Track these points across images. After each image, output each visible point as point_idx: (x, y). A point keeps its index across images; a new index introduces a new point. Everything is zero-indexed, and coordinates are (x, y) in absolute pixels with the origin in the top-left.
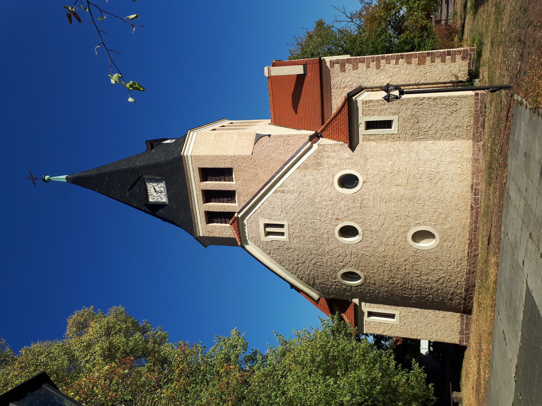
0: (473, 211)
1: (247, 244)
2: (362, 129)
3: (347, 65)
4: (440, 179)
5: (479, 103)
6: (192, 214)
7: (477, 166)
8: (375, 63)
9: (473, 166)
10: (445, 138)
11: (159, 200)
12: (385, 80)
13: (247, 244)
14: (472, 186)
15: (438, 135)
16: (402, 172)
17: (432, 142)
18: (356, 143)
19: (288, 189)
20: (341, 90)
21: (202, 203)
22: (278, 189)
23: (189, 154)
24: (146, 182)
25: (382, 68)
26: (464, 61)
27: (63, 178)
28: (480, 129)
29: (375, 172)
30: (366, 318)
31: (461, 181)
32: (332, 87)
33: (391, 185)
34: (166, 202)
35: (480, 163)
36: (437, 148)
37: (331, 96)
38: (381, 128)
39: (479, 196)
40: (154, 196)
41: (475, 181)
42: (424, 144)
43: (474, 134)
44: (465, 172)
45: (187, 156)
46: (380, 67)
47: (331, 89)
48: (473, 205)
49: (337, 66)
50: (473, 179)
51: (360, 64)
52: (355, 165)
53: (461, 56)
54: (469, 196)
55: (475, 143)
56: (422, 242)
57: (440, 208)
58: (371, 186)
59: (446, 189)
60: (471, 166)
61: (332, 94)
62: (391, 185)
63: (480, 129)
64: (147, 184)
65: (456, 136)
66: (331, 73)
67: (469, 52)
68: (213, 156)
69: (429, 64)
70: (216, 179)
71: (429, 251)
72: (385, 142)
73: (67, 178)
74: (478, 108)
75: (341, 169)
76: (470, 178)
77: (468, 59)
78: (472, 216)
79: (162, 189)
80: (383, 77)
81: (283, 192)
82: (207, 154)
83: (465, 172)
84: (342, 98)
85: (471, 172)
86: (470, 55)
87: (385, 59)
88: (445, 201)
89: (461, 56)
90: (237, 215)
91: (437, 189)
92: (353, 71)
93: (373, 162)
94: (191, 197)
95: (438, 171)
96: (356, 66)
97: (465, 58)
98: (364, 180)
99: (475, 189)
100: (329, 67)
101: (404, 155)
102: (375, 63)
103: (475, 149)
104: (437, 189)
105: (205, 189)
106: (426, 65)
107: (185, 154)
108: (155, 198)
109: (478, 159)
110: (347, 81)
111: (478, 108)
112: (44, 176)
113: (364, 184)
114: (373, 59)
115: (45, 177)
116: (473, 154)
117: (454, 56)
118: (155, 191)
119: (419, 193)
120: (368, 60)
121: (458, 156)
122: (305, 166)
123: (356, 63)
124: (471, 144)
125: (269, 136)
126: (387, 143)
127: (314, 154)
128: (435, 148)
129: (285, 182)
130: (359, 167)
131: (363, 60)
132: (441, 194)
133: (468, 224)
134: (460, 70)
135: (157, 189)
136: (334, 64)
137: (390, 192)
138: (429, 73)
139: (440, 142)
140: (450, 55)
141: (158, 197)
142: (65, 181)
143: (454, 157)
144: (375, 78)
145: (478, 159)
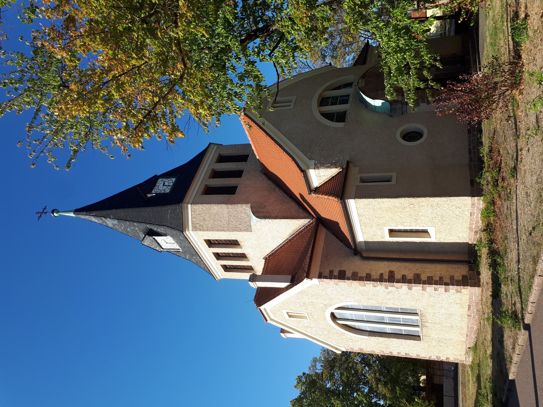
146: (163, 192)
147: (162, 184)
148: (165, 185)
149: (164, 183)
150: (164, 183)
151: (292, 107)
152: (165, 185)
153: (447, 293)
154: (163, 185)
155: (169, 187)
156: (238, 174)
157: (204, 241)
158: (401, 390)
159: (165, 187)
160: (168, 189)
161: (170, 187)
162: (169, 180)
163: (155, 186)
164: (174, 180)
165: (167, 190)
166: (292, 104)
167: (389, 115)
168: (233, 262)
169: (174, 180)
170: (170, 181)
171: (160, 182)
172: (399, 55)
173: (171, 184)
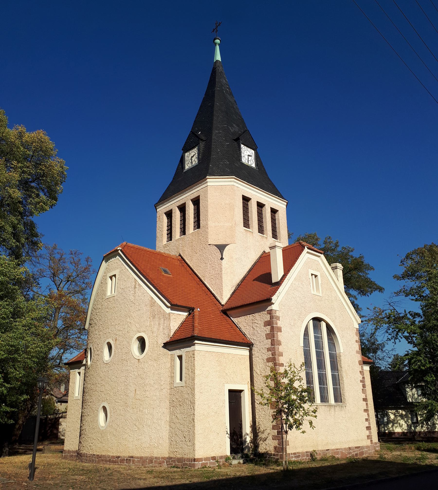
0: (116, 459)
1: (106, 262)
2: (178, 352)
3: (269, 327)
4: (138, 428)
5: (189, 463)
6: (169, 198)
7: (147, 462)
8: (271, 356)
9: (147, 458)
10: (170, 432)
11: (187, 162)
12: (259, 368)
13: (106, 262)
14: (132, 457)
15: (172, 425)
16: (145, 394)
17: (168, 420)
18: (169, 348)
19: (137, 291)
20: (251, 324)
21: (177, 205)
22: (137, 282)
23: (209, 184)
24: (197, 146)
25: (267, 364)
26: (273, 449)
27: (218, 57)
28: (174, 464)
29: (146, 369)
30: (77, 371)
31: (137, 447)
32: (253, 315)
33: (136, 385)
34: (185, 169)
35: (149, 464)
36: (163, 425)
37: (247, 315)
38: (317, 360)
39: (125, 464)
40: (189, 157)
41: (136, 459)
42: (167, 411)
43: (171, 458)
44: (143, 451)
45: (207, 182)
46: (268, 362)
47: (252, 314)
48: (120, 458)
49: (268, 318)
50: (137, 458)
51: (270, 340)
52: (151, 350)
53: (277, 445)
54: (125, 454)
55: (165, 459)
56: (105, 415)
57: (120, 430)
58: (136, 367)
59: (132, 434)
60: (147, 455)
61: (248, 316)
62: (136, 385)
63: (174, 464)
64: (197, 148)
65: (171, 442)
66: (263, 312)
67: (279, 454)
68: (207, 207)
69: (271, 413)
70: (195, 214)
71: (97, 421)
72: (169, 375)
73: (217, 61)
74: (186, 462)
75: (149, 337)
76: (138, 455)
77: (275, 453)
78: (113, 457)
79: (194, 163)
80: (261, 366)
81: (135, 287)
82: (209, 201)
83: (143, 451)
84: (246, 326)
85: (143, 456)
86: (277, 455)
87: (274, 366)
88: (123, 433)
89: (277, 445)
90: (119, 249)
91: (132, 425)
92: (265, 334)
93: (154, 366)
94: (183, 193)
95: (144, 426)
96: (269, 337)
97: (276, 449)
98: (140, 360)
99: (130, 460)
100: (267, 309)
101: (158, 394)
102: (271, 356)
103: (161, 460)
104: (132, 425)
105: (186, 206)
106: (270, 410)
107: (208, 180)
108: (188, 158)
109: (152, 463)
110: (257, 329)
111: (186, 462)
112: (218, 38)
113: (137, 361)
114: (274, 354)
115: (219, 39)
116: (156, 458)
117: (277, 438)
118: (192, 157)
119: (129, 410)
120: (273, 349)
121: (155, 444)
122: (153, 303)
123: (270, 337)
124: (165, 456)
125: (222, 259)
126: (169, 378)
127: (162, 311)
128: (163, 423)
129: (142, 288)
130: (150, 354)
131: (273, 343)
132: (128, 430)
133: (109, 454)
134: (266, 445)
135: (193, 159)
136: (270, 314)
137: (131, 384)
138: (264, 413)
139: (168, 427)
140: (278, 435)
141: (188, 161)
142: (215, 61)
143: (155, 440)
144: (260, 358)
145: (152, 463)
146: (242, 155)
147: (249, 154)
148: (249, 157)
149: (250, 156)
150: (250, 156)
151: (312, 292)
152: (249, 157)
153: (366, 429)
154: (248, 155)
155: (247, 160)
156: (261, 230)
157: (183, 202)
158: (25, 401)
159: (247, 157)
160: (245, 160)
161: (247, 162)
162: (253, 160)
163: (248, 147)
164: (254, 165)
165: (244, 159)
166: (315, 293)
167: (50, 444)
168: (267, 218)
169: (254, 165)
170: (252, 162)
171: (251, 152)
172: (424, 426)
173: (250, 163)
